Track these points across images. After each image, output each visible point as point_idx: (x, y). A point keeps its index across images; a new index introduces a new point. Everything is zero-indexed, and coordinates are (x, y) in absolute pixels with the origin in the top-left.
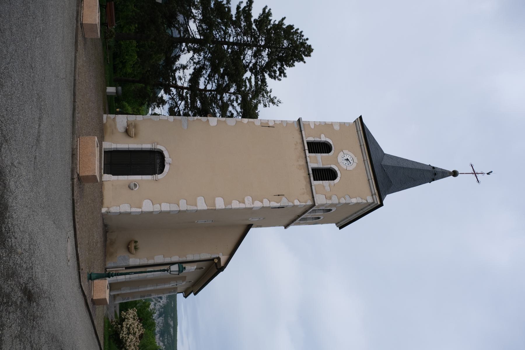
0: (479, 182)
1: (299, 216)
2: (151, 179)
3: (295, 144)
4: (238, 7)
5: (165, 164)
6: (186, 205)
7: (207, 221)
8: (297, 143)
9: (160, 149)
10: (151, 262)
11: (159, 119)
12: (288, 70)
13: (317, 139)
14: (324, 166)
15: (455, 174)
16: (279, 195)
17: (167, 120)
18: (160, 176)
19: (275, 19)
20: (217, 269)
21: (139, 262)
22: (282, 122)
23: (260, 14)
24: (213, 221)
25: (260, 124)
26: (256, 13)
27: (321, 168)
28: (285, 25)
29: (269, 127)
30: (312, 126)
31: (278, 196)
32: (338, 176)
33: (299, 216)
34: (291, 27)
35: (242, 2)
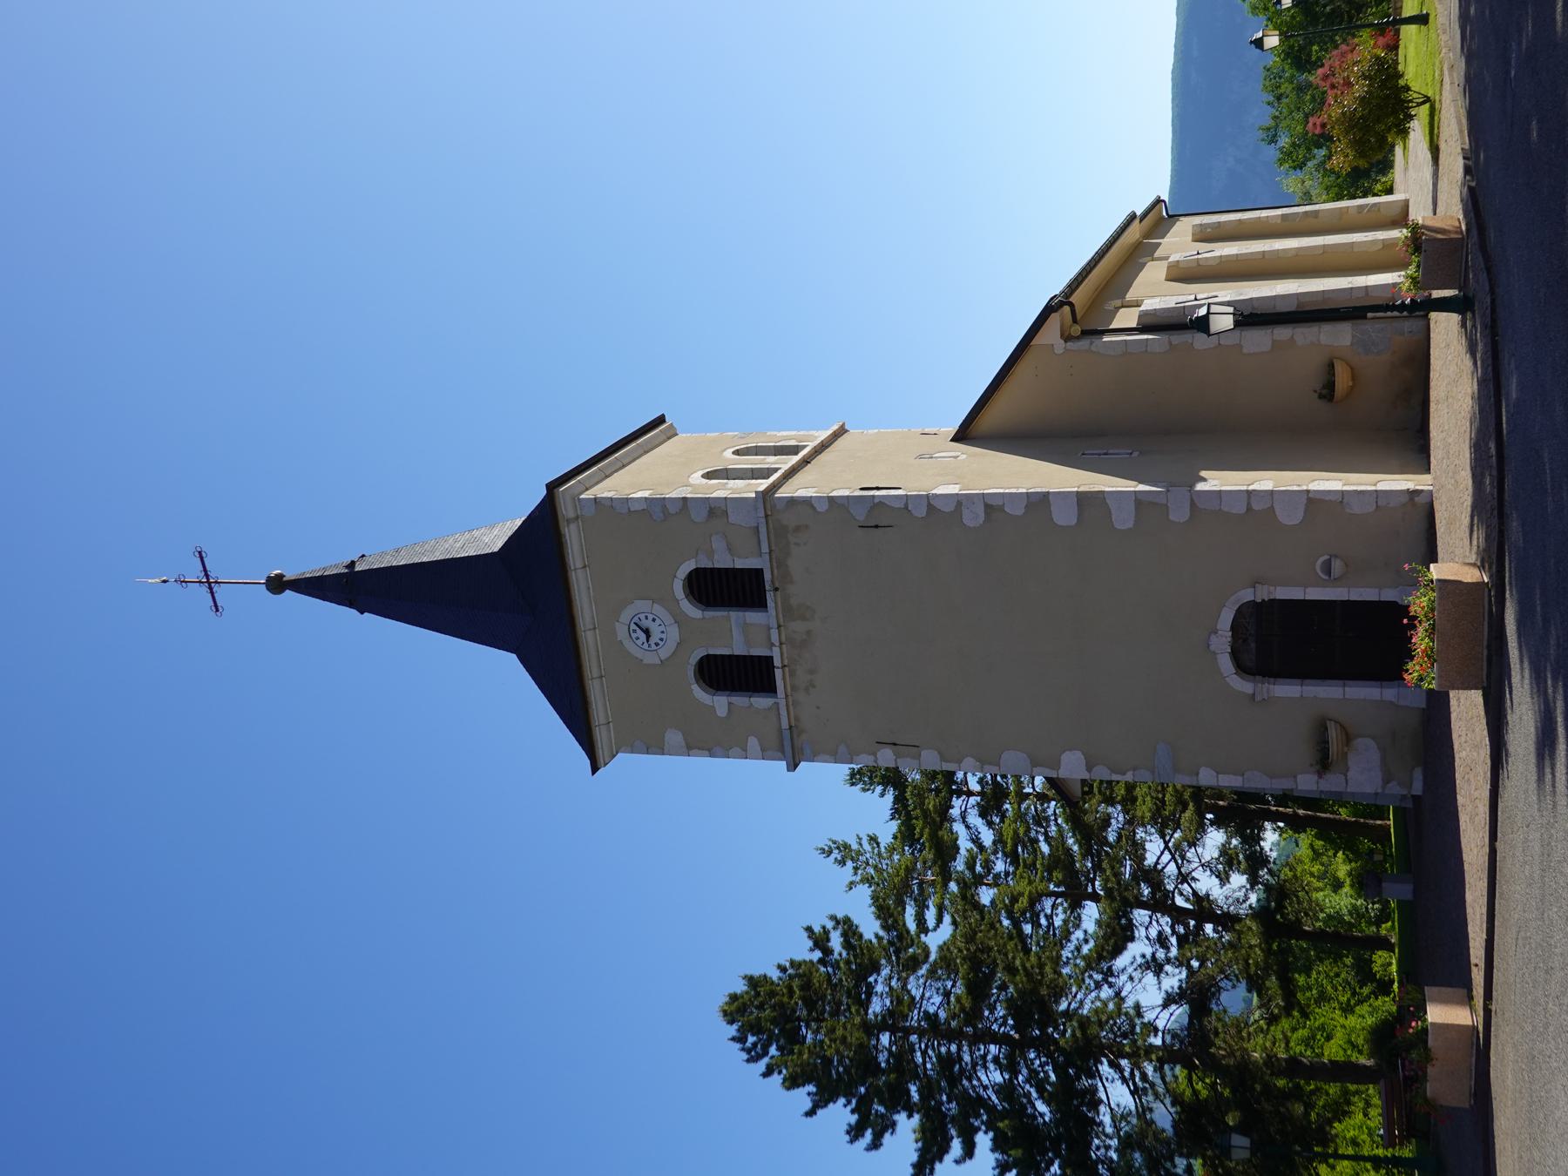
0: (197, 554)
1: (806, 461)
2: (1278, 588)
3: (814, 687)
4: (969, 1151)
5: (1230, 633)
6: (1169, 505)
7: (1099, 455)
8: (807, 690)
9: (1244, 682)
10: (1283, 333)
11: (1245, 776)
12: (804, 951)
13: (740, 700)
14: (725, 613)
15: (277, 585)
16: (877, 527)
17: (1218, 773)
18: (1247, 595)
19: (840, 1114)
20: (1071, 305)
21: (1320, 332)
22: (852, 759)
23: (892, 1133)
24: (1083, 454)
25: (922, 753)
26: (906, 1132)
27: (734, 608)
28: (809, 1094)
29: (895, 744)
30: (753, 742)
31: (880, 525)
32: (681, 583)
33: (806, 461)
34: (792, 1083)
35: (957, 1162)
